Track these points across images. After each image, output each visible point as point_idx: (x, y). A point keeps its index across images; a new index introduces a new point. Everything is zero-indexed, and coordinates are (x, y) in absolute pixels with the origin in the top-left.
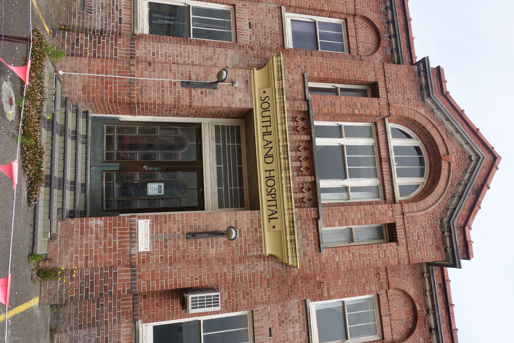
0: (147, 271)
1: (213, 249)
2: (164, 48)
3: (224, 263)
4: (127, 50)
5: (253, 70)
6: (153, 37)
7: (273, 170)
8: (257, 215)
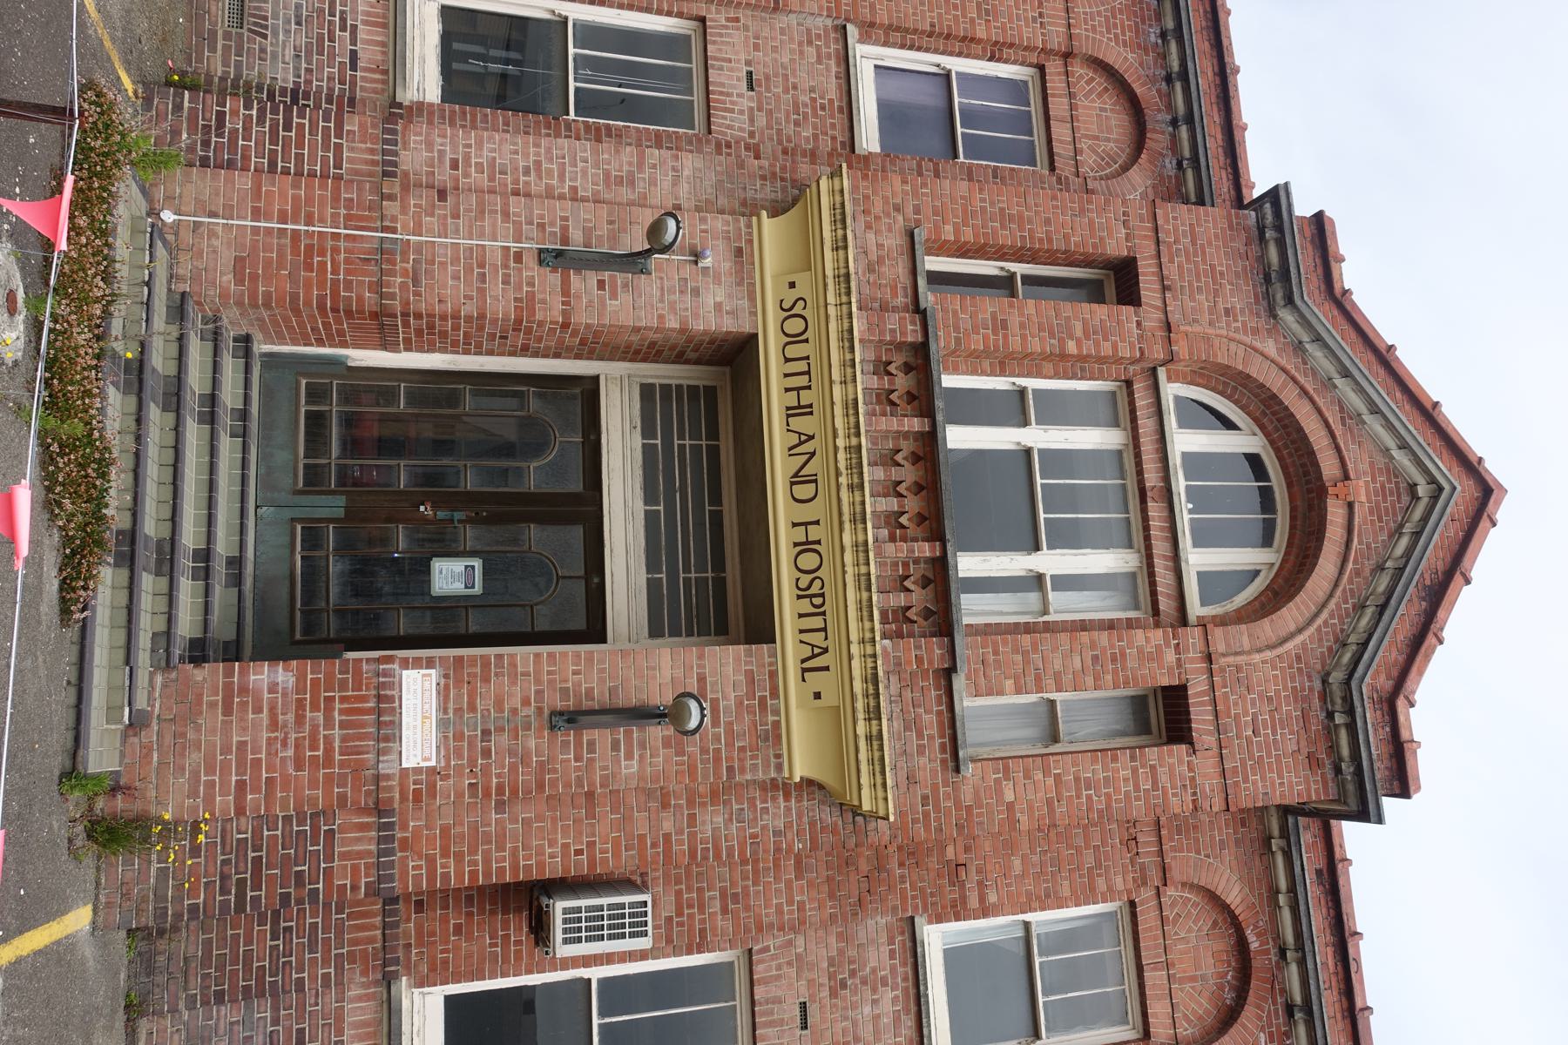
0: (428, 827)
1: (634, 759)
3: (665, 805)
4: (372, 151)
5: (759, 216)
6: (453, 112)
7: (817, 523)
8: (767, 660)
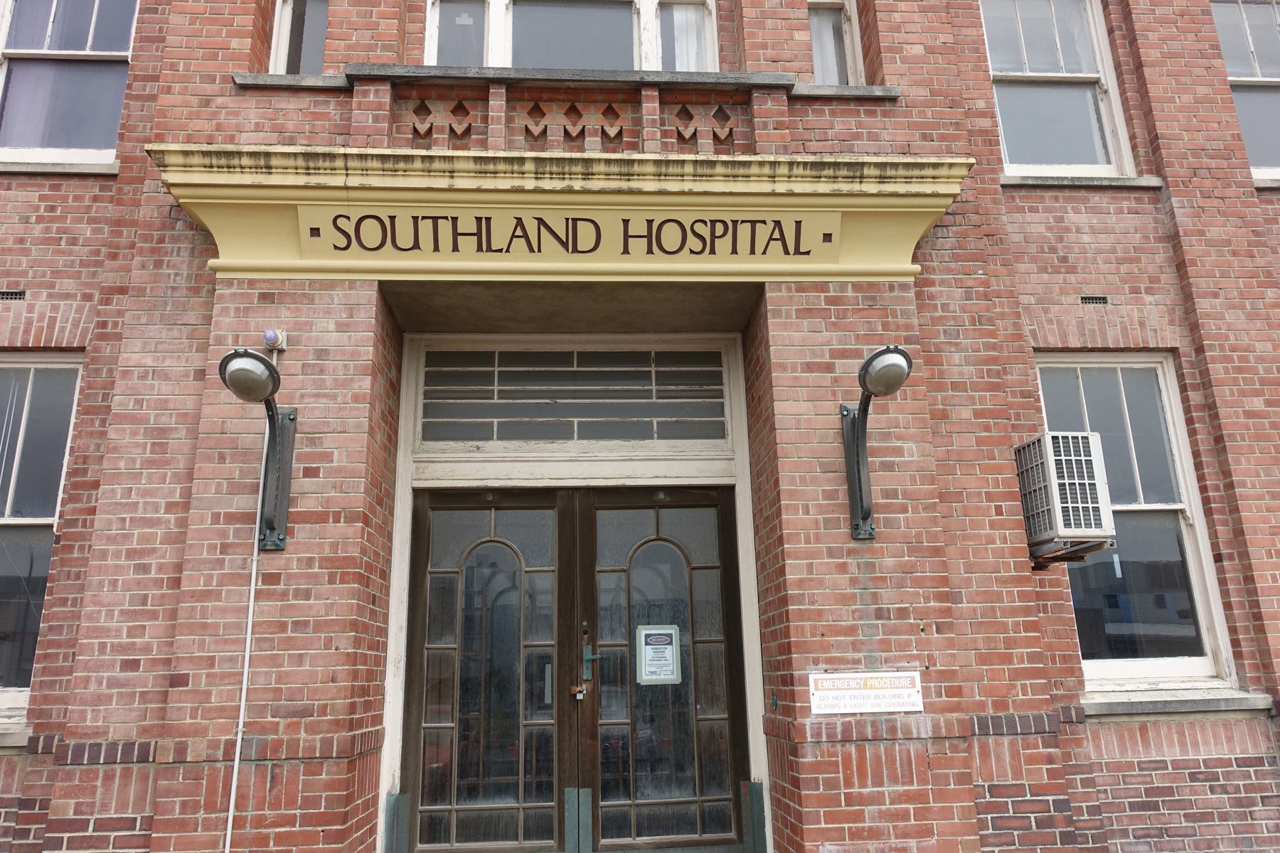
0: (981, 679)
2: (102, 623)
3: (944, 415)
4: (109, 778)
5: (215, 270)
6: (45, 671)
7: (626, 222)
8: (784, 293)
